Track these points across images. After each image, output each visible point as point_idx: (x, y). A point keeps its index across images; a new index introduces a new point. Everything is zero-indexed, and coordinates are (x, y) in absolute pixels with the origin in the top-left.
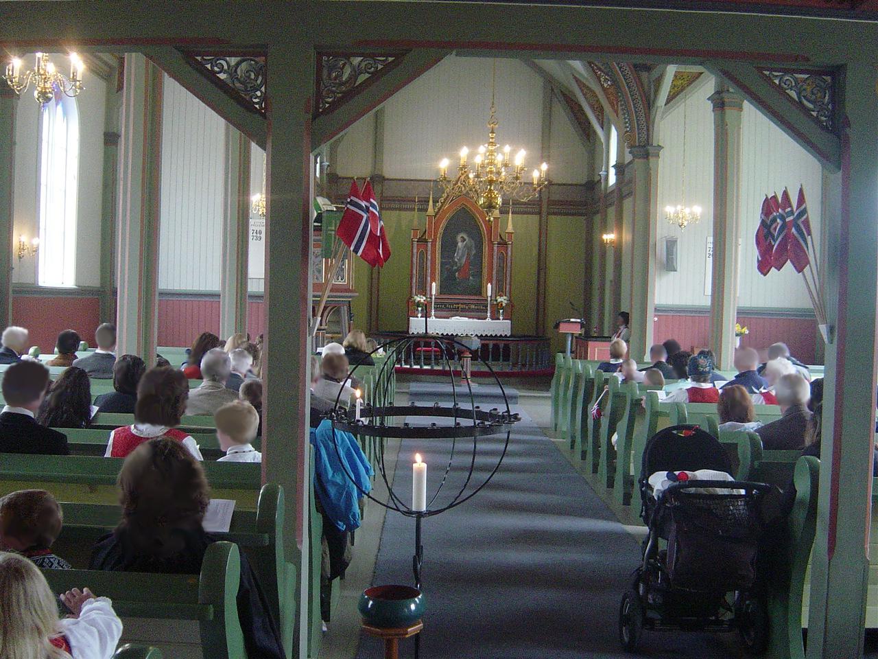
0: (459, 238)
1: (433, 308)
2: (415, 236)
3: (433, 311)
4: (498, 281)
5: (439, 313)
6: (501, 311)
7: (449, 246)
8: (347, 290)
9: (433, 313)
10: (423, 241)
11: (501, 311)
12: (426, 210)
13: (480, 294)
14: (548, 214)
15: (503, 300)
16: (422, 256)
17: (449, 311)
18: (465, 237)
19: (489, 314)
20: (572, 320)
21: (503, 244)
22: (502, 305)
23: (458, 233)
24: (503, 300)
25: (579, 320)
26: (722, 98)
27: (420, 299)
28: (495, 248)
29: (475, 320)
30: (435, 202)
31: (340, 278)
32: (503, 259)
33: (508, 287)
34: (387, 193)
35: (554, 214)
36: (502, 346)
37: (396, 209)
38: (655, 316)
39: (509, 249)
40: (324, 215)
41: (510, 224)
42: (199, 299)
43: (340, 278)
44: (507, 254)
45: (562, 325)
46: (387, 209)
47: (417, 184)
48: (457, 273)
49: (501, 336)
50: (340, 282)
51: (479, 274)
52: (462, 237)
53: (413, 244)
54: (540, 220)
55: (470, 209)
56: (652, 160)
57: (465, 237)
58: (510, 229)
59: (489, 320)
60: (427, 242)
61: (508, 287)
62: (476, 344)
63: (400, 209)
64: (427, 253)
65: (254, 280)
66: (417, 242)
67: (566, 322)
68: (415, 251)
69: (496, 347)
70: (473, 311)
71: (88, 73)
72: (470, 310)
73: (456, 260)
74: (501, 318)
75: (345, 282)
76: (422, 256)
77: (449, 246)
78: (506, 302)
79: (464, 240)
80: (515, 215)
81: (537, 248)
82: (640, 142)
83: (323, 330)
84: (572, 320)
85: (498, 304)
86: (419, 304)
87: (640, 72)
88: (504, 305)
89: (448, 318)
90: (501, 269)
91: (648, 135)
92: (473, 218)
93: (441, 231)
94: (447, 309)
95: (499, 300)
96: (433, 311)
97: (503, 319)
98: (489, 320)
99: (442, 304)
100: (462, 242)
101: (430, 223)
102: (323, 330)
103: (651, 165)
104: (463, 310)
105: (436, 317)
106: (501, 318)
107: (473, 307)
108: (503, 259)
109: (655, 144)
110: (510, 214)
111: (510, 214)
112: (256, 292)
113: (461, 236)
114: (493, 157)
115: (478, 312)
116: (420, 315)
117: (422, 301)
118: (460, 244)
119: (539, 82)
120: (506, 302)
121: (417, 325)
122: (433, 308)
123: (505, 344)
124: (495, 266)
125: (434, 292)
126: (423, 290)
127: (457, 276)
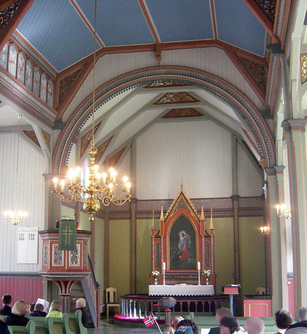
0: (181, 234)
1: (164, 279)
2: (153, 234)
3: (164, 280)
4: (206, 260)
5: (169, 282)
6: (207, 279)
7: (175, 239)
8: (80, 270)
9: (164, 282)
10: (158, 237)
11: (207, 279)
12: (159, 218)
13: (196, 270)
14: (239, 216)
15: (208, 272)
16: (158, 246)
17: (177, 280)
18: (185, 233)
19: (199, 282)
20: (232, 285)
21: (208, 236)
22: (207, 275)
23: (179, 231)
24: (208, 272)
25: (237, 286)
26: (289, 124)
27: (156, 273)
28: (203, 240)
29: (192, 286)
30: (165, 212)
31: (74, 263)
32: (208, 245)
33: (212, 264)
34: (140, 209)
35: (243, 216)
36: (210, 303)
37: (144, 218)
38: (289, 281)
39: (212, 240)
40: (60, 223)
41: (211, 224)
42: (22, 278)
43: (74, 263)
44: (211, 243)
45: (225, 289)
46: (139, 218)
47: (142, 202)
48: (180, 256)
49: (206, 295)
50: (75, 265)
51: (194, 256)
52: (183, 234)
53: (152, 239)
54: (234, 221)
55: (187, 216)
56: (278, 175)
57: (185, 233)
58: (211, 227)
59: (199, 285)
60: (160, 237)
61: (212, 264)
62: (173, 302)
63: (147, 218)
64: (161, 244)
65: (22, 264)
66: (155, 237)
67: (228, 287)
68: (154, 243)
69: (200, 303)
70: (190, 279)
71: (115, 167)
72: (189, 279)
73: (179, 248)
74: (207, 284)
75: (78, 265)
76: (158, 246)
77: (175, 239)
78: (210, 273)
79: (183, 235)
80: (214, 218)
81: (233, 238)
82: (270, 165)
83: (67, 296)
84: (232, 285)
85: (204, 275)
86: (155, 277)
87: (267, 120)
88: (208, 275)
89: (174, 285)
90: (208, 252)
91: (275, 160)
92: (189, 222)
93: (169, 231)
94: (172, 279)
95: (205, 272)
96: (164, 280)
97: (208, 285)
98: (199, 285)
99: (171, 276)
100: (183, 236)
101: (162, 226)
102: (67, 296)
103: (278, 179)
104: (184, 279)
105: (166, 284)
106: (207, 284)
107: (190, 277)
108: (208, 245)
109: (279, 165)
110: (211, 217)
111: (211, 217)
112: (13, 272)
113: (182, 233)
114: (93, 175)
115: (193, 280)
116: (156, 283)
117: (157, 274)
118: (181, 238)
119: (228, 135)
120: (210, 273)
121: (154, 290)
122: (164, 279)
123: (212, 302)
124: (203, 251)
125: (164, 268)
126: (159, 268)
127: (180, 258)
